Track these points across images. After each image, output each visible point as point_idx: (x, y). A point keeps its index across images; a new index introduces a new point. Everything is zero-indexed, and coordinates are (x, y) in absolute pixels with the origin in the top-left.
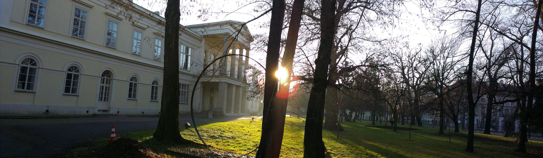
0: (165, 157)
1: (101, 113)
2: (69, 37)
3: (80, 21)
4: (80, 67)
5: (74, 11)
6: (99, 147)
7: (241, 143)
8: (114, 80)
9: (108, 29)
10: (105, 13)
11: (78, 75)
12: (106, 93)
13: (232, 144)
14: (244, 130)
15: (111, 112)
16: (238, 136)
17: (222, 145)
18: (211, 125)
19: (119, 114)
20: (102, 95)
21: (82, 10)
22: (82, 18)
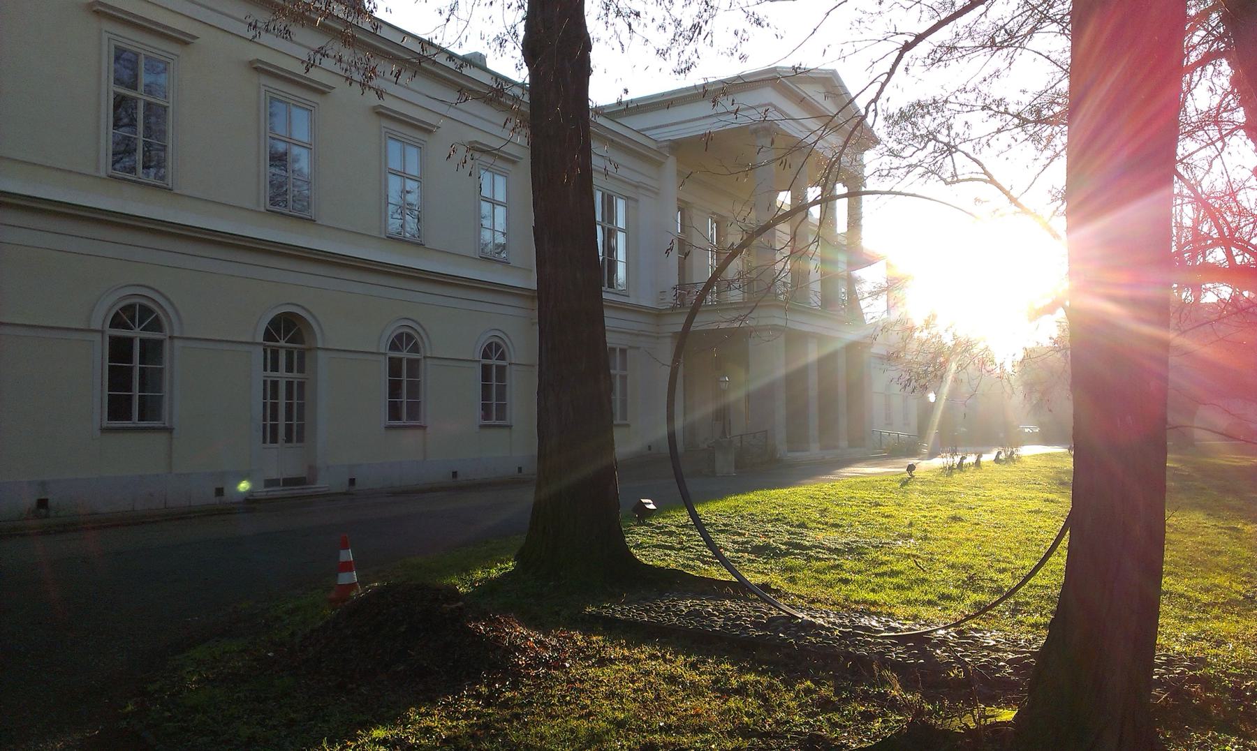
0: (575, 643)
1: (278, 491)
2: (260, 212)
3: (141, 105)
4: (164, 310)
5: (107, 64)
6: (293, 634)
7: (902, 573)
8: (320, 354)
9: (269, 134)
10: (251, 63)
11: (159, 343)
12: (289, 407)
13: (858, 577)
14: (887, 517)
15: (324, 483)
16: (875, 542)
17: (813, 581)
18: (741, 503)
19: (357, 487)
20: (274, 416)
21: (146, 57)
22: (149, 93)
